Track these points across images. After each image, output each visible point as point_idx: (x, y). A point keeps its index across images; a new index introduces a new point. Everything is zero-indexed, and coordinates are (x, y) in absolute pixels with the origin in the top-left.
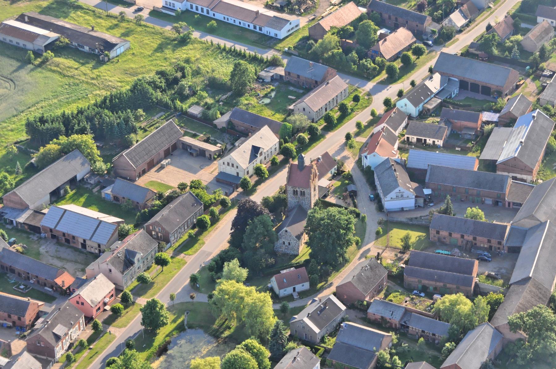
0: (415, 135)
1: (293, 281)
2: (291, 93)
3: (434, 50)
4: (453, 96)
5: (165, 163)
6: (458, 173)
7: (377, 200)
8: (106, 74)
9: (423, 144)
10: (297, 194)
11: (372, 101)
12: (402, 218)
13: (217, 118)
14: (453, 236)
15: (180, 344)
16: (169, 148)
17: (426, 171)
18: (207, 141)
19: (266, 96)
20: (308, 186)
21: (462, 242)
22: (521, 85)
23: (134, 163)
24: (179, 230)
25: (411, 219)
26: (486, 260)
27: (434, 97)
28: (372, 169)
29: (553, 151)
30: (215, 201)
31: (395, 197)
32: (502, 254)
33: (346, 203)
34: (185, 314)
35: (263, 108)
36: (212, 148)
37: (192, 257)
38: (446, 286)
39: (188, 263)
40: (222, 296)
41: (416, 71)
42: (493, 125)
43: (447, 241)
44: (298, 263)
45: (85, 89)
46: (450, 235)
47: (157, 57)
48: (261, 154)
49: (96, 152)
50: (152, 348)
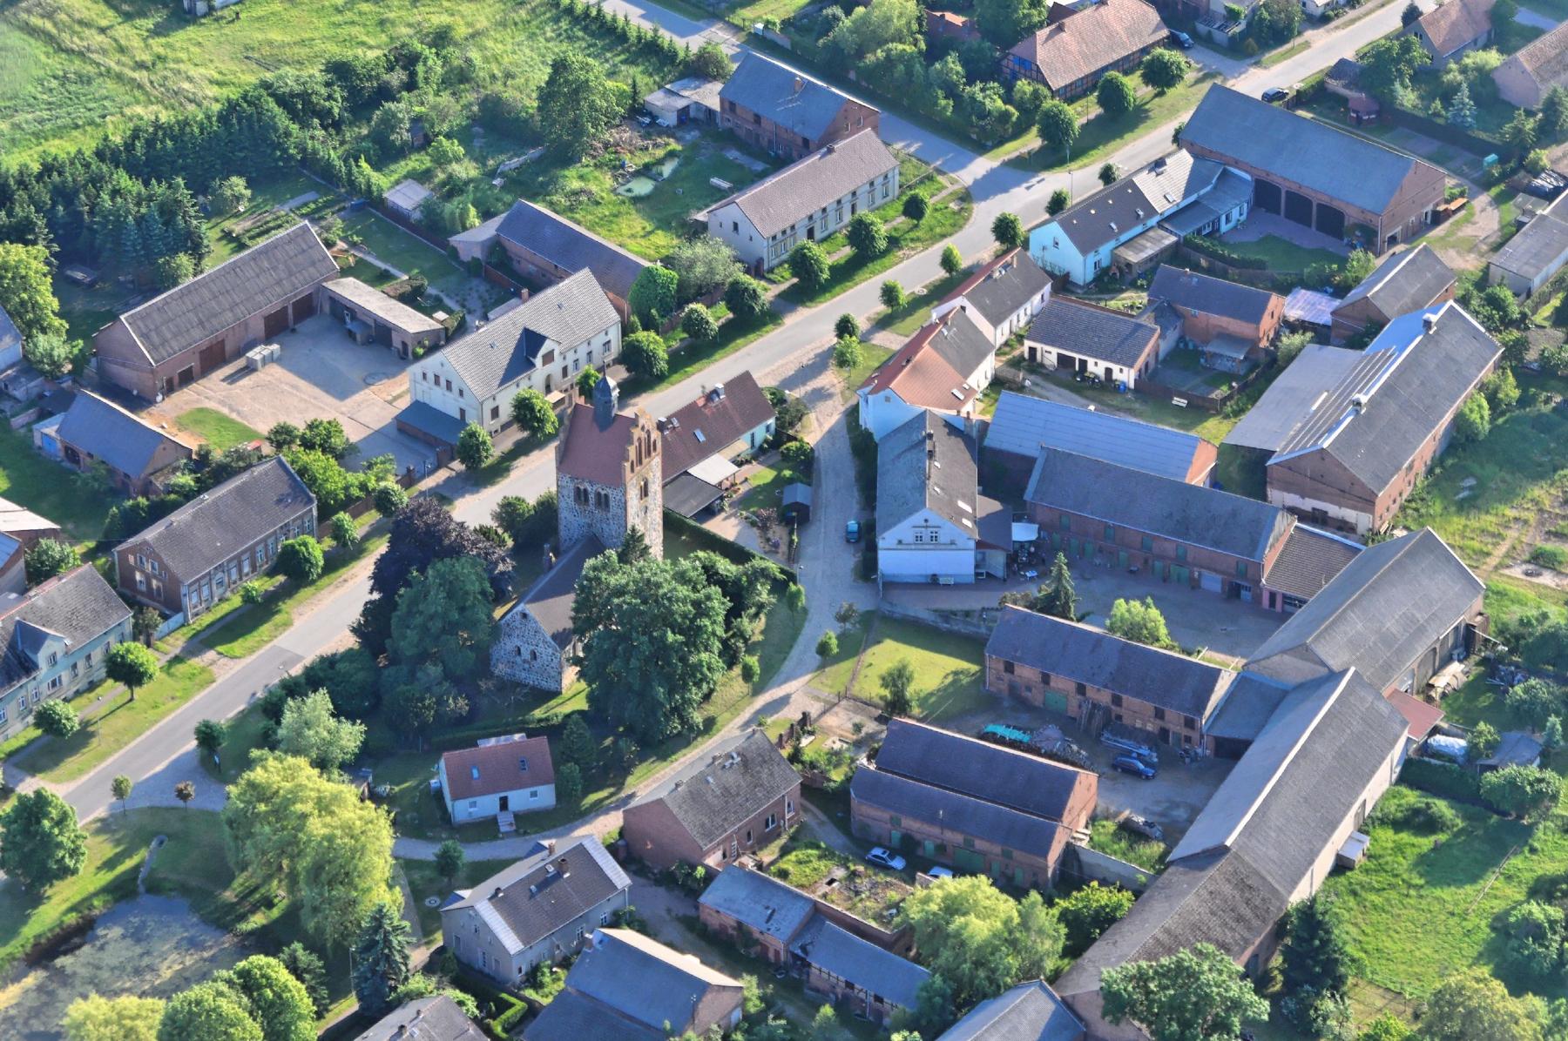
0: (1053, 344)
1: (518, 772)
2: (722, 169)
3: (1220, 74)
4: (1224, 228)
5: (258, 357)
6: (1129, 482)
7: (865, 540)
8: (183, 56)
9: (1076, 374)
10: (586, 500)
11: (967, 219)
12: (919, 607)
13: (465, 228)
14: (1052, 684)
15: (102, 941)
16: (285, 309)
17: (1030, 462)
18: (411, 298)
19: (645, 171)
20: (620, 483)
21: (1080, 706)
22: (1448, 214)
23: (153, 348)
24: (220, 575)
25: (947, 615)
26: (1137, 774)
27: (1160, 225)
28: (876, 438)
29: (1473, 441)
30: (362, 494)
31: (911, 539)
32: (1195, 758)
33: (768, 540)
34: (154, 844)
35: (623, 209)
36: (410, 321)
37: (238, 666)
38: (973, 846)
39: (219, 681)
40: (249, 802)
41: (1141, 136)
42: (1309, 335)
43: (1036, 697)
44: (547, 719)
45: (106, 98)
46: (1046, 679)
47: (360, 13)
48: (548, 358)
49: (49, 301)
50: (13, 942)
